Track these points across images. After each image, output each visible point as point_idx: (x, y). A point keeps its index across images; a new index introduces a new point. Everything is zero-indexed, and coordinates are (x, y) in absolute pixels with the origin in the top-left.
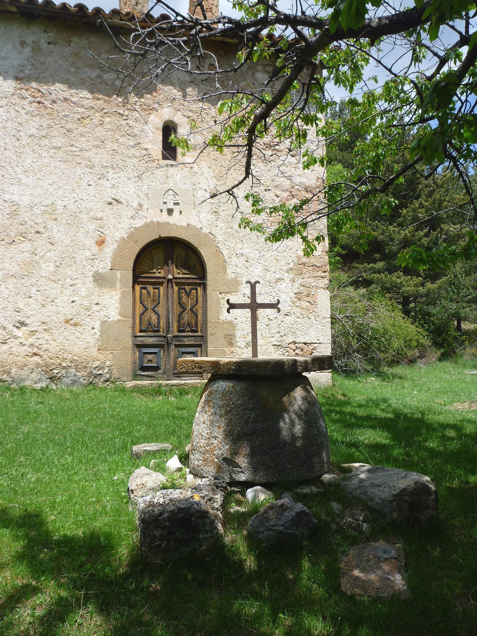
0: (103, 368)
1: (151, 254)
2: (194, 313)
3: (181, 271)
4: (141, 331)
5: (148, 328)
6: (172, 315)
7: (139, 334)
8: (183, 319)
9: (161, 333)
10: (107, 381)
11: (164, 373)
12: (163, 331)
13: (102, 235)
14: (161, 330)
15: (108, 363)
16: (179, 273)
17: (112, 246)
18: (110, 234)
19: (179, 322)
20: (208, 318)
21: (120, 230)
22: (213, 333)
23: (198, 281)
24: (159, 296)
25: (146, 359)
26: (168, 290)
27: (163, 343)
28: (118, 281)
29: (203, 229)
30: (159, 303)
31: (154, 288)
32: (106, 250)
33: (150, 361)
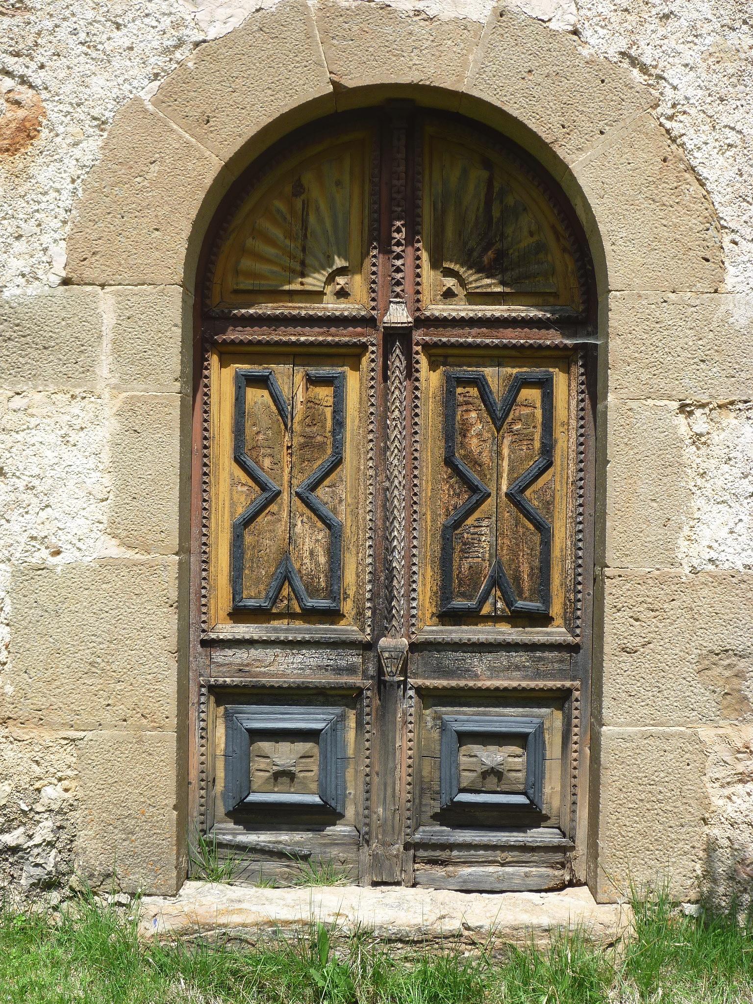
0: (27, 817)
1: (299, 189)
2: (528, 515)
3: (462, 283)
4: (239, 614)
5: (275, 600)
6: (410, 530)
7: (228, 630)
8: (466, 551)
9: (348, 628)
10: (50, 884)
11: (362, 839)
12: (360, 614)
13: (25, 94)
14: (348, 607)
15: (52, 793)
16: (449, 294)
17: (77, 152)
18: (67, 88)
19: (445, 563)
20: (611, 556)
21: (116, 62)
22: (636, 642)
23: (553, 338)
24: (339, 423)
25: (262, 763)
26: (386, 392)
27: (356, 680)
28: (106, 346)
29: (587, 33)
30: (337, 463)
31: (312, 381)
32: (44, 174)
33: (284, 776)
